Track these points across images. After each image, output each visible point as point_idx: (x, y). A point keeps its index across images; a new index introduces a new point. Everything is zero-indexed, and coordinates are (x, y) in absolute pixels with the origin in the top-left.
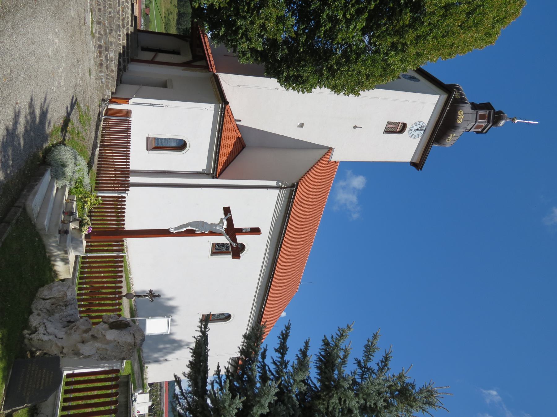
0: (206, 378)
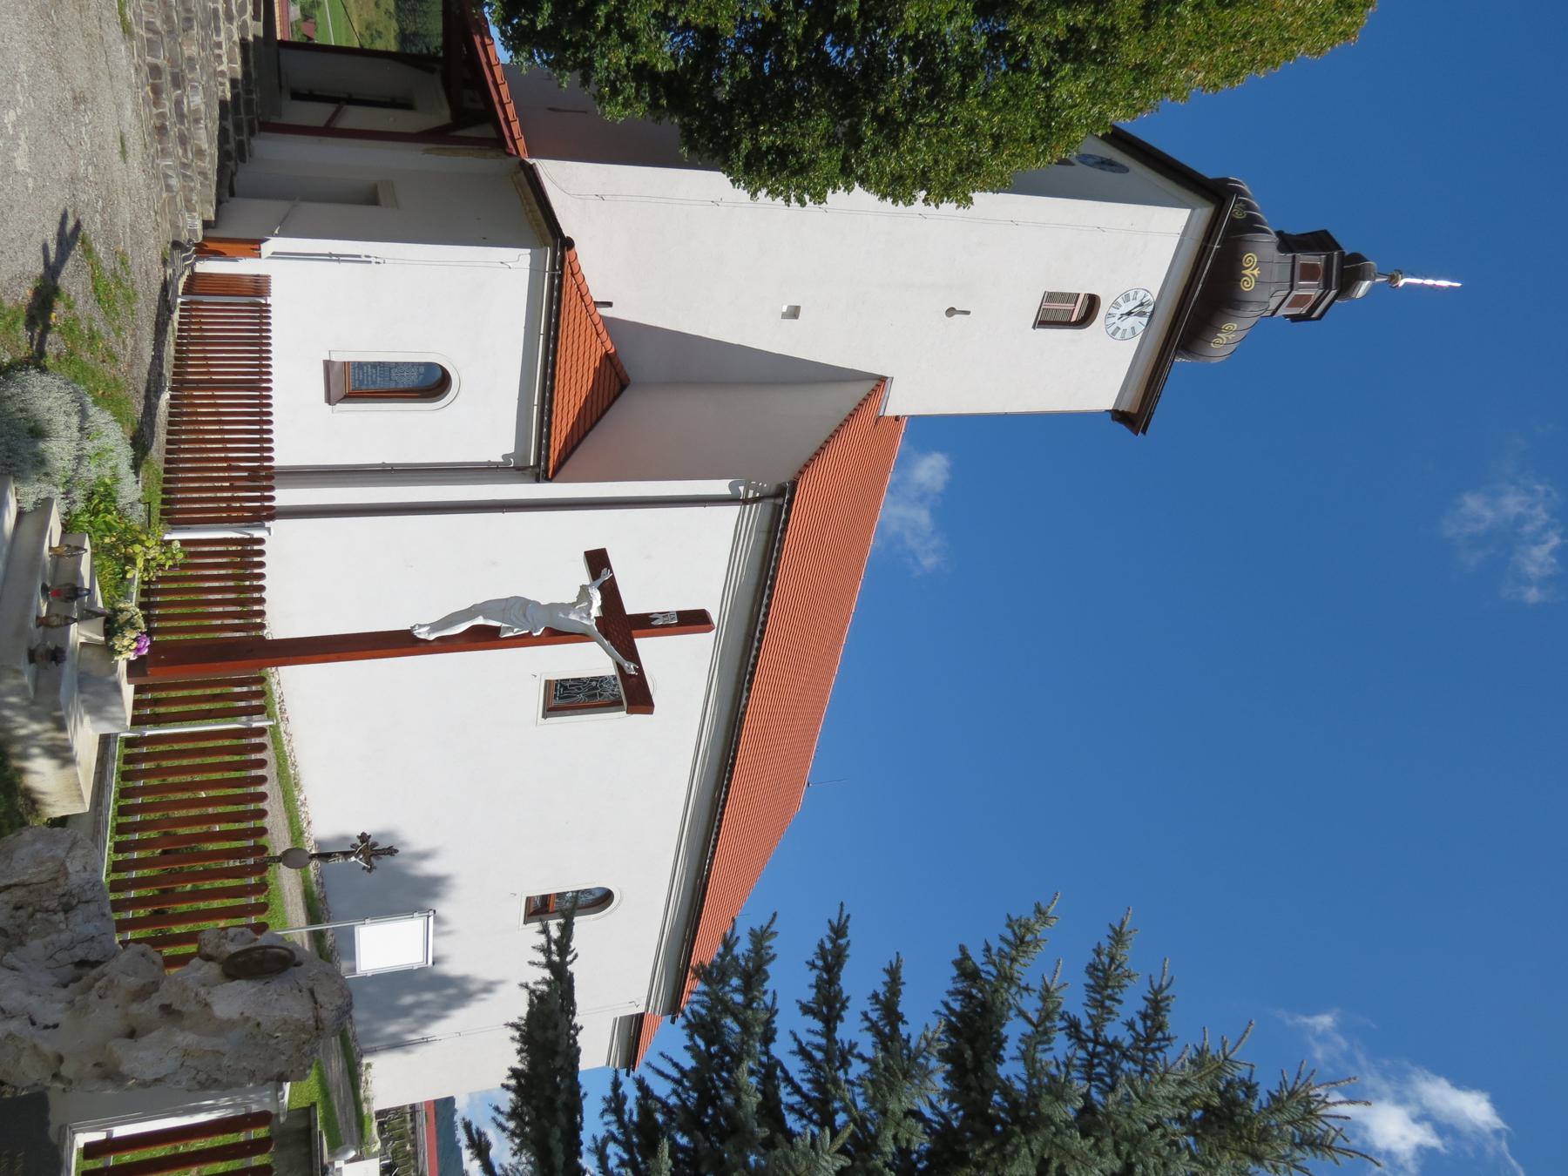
0: (574, 1129)
